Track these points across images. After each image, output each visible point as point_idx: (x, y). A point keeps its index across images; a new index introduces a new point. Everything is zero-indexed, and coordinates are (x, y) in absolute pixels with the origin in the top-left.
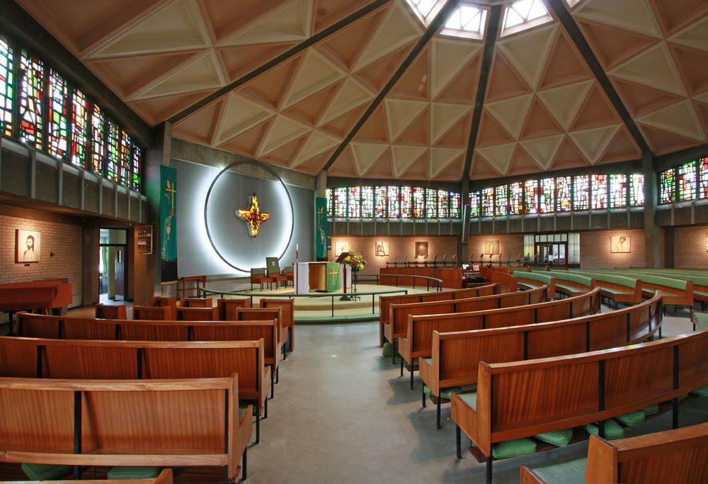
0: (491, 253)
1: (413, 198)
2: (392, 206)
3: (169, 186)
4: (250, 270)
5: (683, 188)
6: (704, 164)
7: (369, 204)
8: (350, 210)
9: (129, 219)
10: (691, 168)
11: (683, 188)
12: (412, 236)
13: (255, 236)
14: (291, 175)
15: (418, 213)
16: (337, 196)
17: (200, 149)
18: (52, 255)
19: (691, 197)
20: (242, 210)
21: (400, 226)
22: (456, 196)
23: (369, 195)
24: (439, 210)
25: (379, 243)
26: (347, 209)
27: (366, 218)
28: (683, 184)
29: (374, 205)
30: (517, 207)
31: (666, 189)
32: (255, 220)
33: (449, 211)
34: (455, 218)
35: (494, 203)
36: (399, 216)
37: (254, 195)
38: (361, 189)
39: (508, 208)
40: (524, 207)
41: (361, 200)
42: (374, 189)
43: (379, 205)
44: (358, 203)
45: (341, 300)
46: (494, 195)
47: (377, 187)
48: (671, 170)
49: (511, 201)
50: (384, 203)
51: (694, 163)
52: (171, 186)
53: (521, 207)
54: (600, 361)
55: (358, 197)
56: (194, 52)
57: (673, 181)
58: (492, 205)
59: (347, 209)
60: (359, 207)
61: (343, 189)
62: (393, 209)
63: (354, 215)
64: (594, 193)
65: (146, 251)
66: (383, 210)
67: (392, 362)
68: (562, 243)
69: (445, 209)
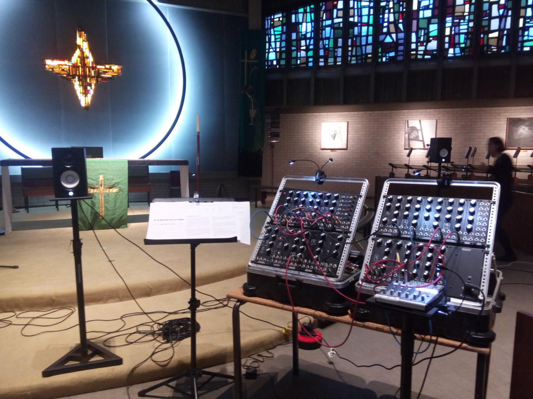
4: (233, 307)
10: (308, 15)
15: (493, 42)
25: (414, 123)
32: (83, 79)
43: (389, 33)
48: (280, 15)
57: (283, 33)
59: (316, 50)
60: (340, 42)
65: (484, 203)
68: (439, 174)
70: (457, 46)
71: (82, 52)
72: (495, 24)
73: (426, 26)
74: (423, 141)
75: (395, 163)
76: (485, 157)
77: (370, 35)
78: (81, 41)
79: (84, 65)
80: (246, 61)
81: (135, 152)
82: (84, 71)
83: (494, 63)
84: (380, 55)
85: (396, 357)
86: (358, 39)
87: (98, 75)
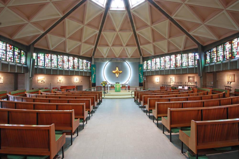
0: (230, 81)
1: (176, 59)
3: (94, 68)
7: (158, 64)
8: (152, 67)
9: (215, 71)
12: (186, 74)
13: (117, 77)
14: (129, 60)
16: (148, 63)
17: (102, 59)
19: (42, 65)
21: (194, 69)
22: (89, 63)
24: (84, 67)
25: (171, 77)
26: (151, 66)
29: (160, 64)
30: (228, 56)
32: (117, 73)
33: (87, 68)
35: (217, 55)
36: (170, 67)
37: (117, 67)
38: (156, 59)
39: (224, 57)
40: (232, 55)
41: (156, 63)
42: (160, 58)
44: (155, 64)
45: (136, 96)
46: (217, 51)
47: (166, 57)
49: (225, 53)
50: (164, 63)
53: (230, 55)
54: (37, 113)
55: (155, 62)
58: (216, 56)
59: (151, 66)
60: (155, 65)
61: (150, 60)
62: (167, 64)
64: (8, 53)
66: (164, 66)
67: (153, 121)
78: (117, 68)
79: (117, 71)
81: (124, 83)
87: (119, 73)
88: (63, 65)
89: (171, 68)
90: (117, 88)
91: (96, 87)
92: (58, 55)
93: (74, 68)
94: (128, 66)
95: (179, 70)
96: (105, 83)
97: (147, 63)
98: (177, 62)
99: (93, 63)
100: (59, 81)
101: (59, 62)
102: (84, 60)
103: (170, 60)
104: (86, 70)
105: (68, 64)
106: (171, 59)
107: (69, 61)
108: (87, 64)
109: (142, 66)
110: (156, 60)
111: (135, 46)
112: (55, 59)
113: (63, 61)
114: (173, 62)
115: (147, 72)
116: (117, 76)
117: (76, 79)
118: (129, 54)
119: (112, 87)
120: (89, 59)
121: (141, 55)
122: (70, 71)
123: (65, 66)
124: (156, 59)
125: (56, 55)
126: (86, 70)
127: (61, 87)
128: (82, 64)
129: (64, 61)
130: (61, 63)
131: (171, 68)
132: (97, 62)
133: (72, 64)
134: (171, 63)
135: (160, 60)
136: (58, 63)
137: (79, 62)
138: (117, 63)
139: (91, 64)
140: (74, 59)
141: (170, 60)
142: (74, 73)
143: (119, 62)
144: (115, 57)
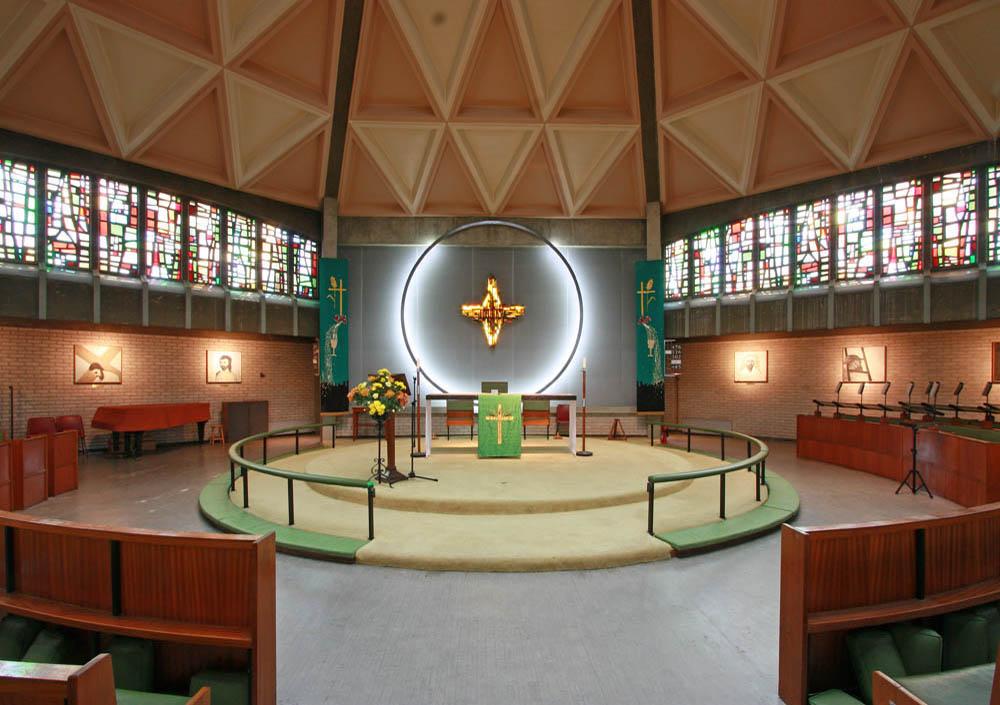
2: (850, 248)
3: (334, 284)
5: (700, 273)
6: (731, 235)
8: (728, 278)
11: (700, 273)
13: (493, 347)
14: (572, 230)
16: (700, 250)
18: (262, 376)
20: (469, 304)
22: (308, 248)
23: (779, 231)
25: (852, 351)
26: (722, 274)
27: (771, 289)
28: (700, 267)
29: (793, 254)
31: (674, 272)
32: (491, 320)
34: (305, 296)
36: (878, 270)
37: (492, 277)
38: (756, 221)
41: (758, 247)
43: (809, 251)
44: (748, 256)
47: (761, 217)
50: (824, 243)
51: (717, 231)
52: (338, 284)
55: (748, 244)
56: (321, 131)
59: (722, 274)
60: (750, 266)
61: (712, 233)
63: (739, 287)
69: (281, 272)
70: (900, 260)
71: (492, 298)
72: (952, 231)
73: (856, 240)
74: (868, 372)
75: (820, 400)
76: (980, 394)
77: (869, 219)
78: (492, 288)
79: (493, 308)
80: (642, 292)
81: (531, 390)
82: (493, 314)
83: (954, 275)
84: (799, 276)
85: (23, 214)
86: (772, 260)
87: (504, 316)
88: (94, 248)
89: (885, 275)
90: (492, 426)
91: (351, 412)
92: (50, 172)
93: (186, 273)
94: (563, 266)
95: (967, 288)
96: (390, 393)
97: (692, 254)
98: (937, 231)
99: (330, 252)
100: (92, 368)
101: (58, 224)
102: (269, 227)
103: (878, 219)
104: (282, 292)
105: (134, 245)
106: (887, 211)
107: (151, 223)
108: (291, 256)
109: (657, 269)
110: (756, 232)
111: (619, 111)
112: (21, 200)
113: (95, 221)
114: (902, 237)
115: (693, 310)
116: (492, 339)
117: (224, 357)
118: (576, 187)
119: (459, 412)
120: (303, 220)
121: (653, 194)
122: (155, 294)
123: (115, 259)
124: (762, 224)
125: (29, 164)
126: (282, 292)
127: (102, 411)
128: (254, 254)
129: (103, 216)
130: (74, 235)
131: (885, 275)
132: (355, 240)
133: (172, 247)
134: (885, 244)
135: (793, 227)
136: (51, 232)
137: (230, 239)
138: (493, 265)
139: (317, 257)
140: (186, 211)
141: (878, 219)
142: (184, 311)
143: (508, 243)
144: (479, 207)
